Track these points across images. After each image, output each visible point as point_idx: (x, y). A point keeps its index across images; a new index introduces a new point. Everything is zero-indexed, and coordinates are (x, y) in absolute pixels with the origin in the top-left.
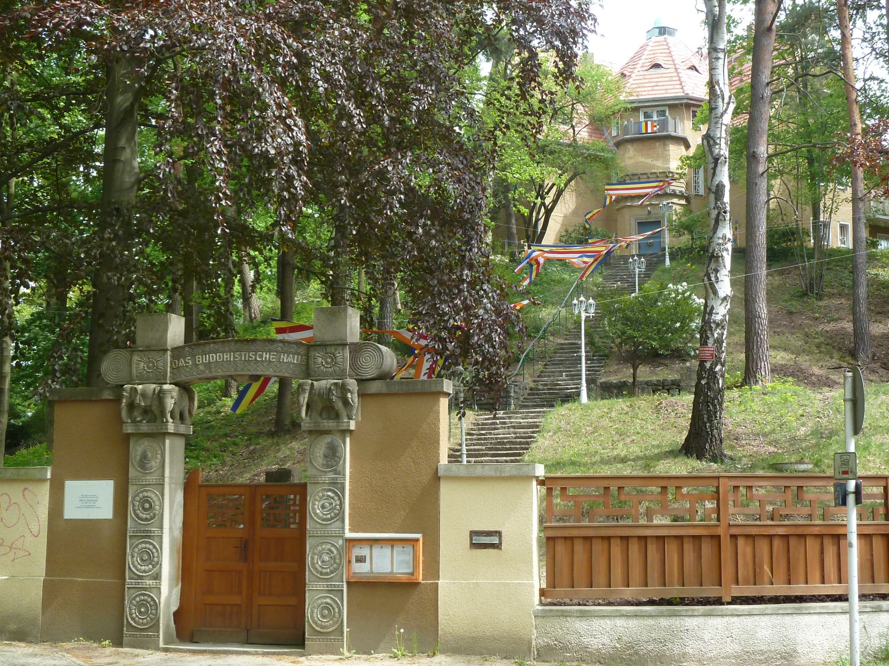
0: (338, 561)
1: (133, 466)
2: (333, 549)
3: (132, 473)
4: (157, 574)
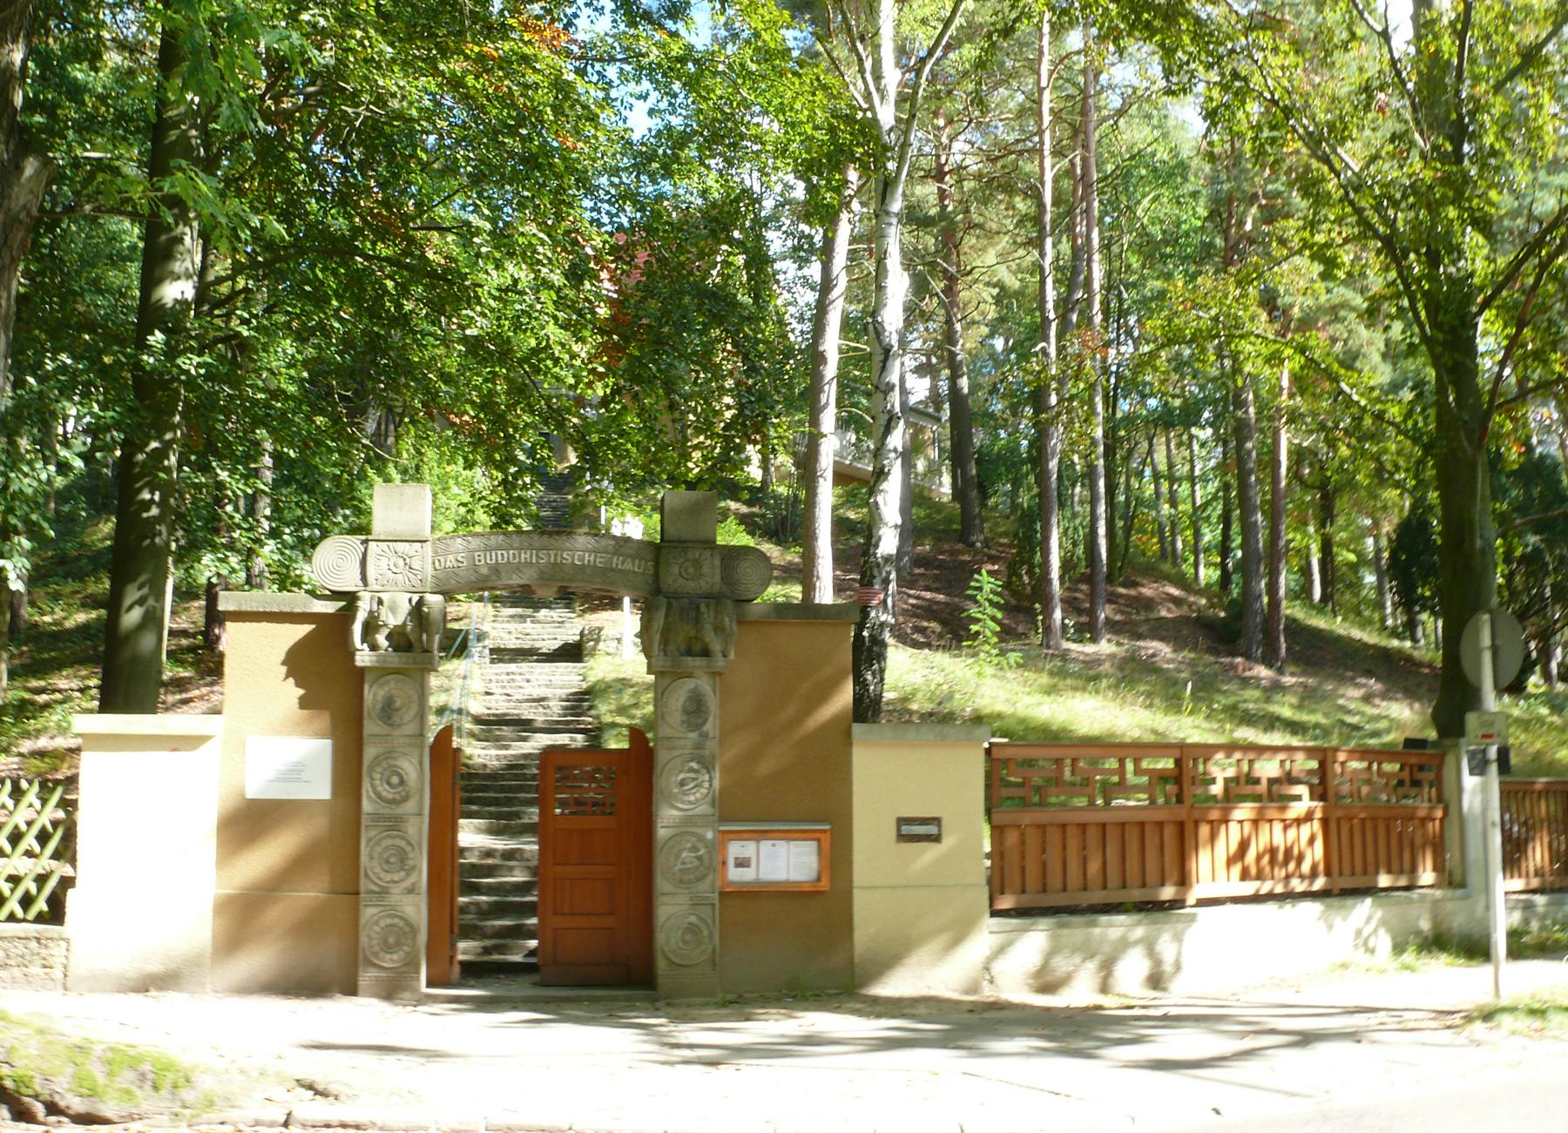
0: (706, 862)
2: (700, 845)
3: (371, 727)
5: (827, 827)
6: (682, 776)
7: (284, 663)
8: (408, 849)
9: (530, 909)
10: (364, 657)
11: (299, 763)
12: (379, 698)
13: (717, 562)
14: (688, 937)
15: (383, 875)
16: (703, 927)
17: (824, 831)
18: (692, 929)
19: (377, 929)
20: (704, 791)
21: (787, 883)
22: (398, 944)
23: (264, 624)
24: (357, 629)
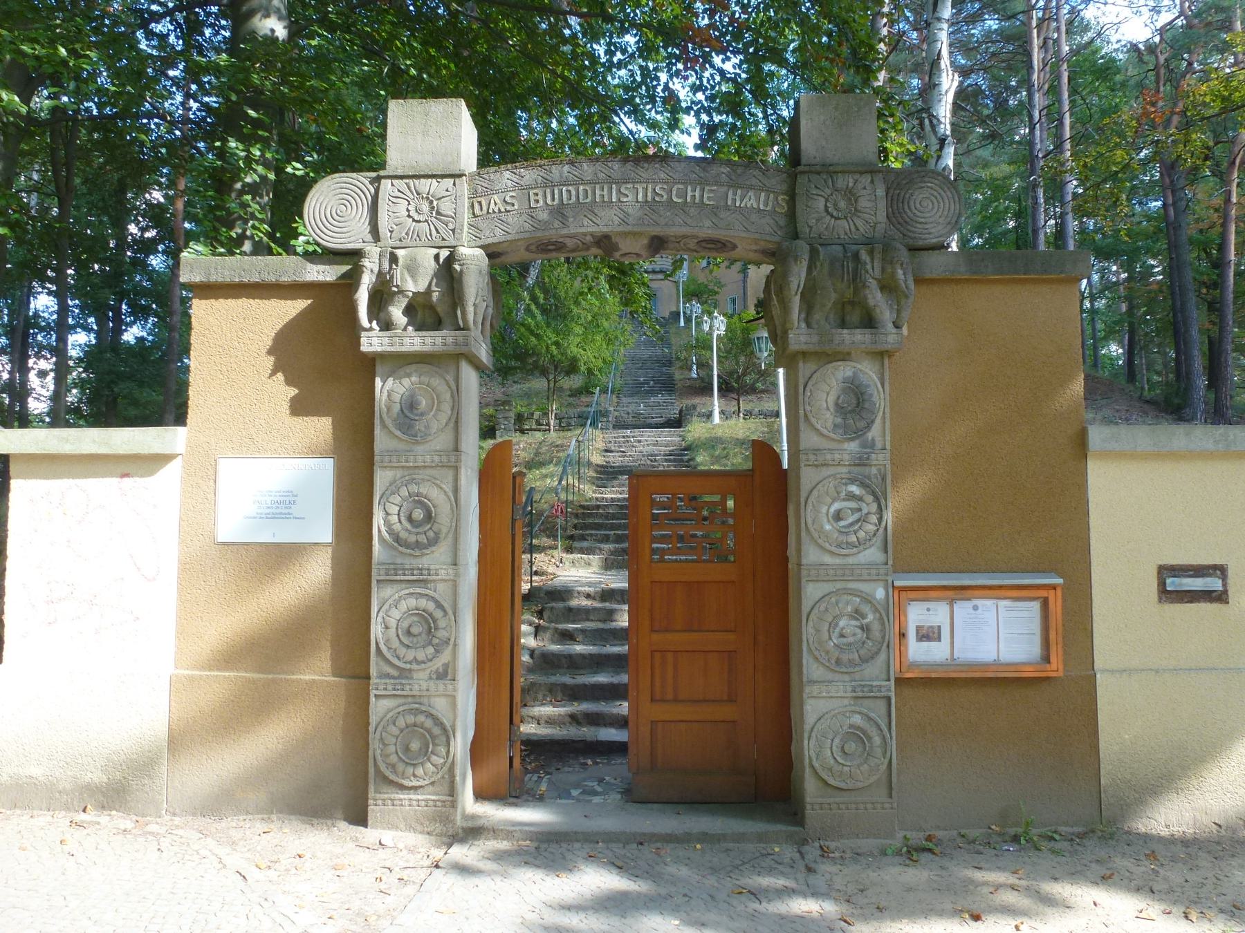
0: (876, 634)
1: (384, 426)
2: (866, 609)
3: (382, 441)
4: (446, 666)
5: (1061, 581)
6: (836, 506)
7: (270, 353)
8: (438, 614)
9: (615, 692)
10: (373, 341)
11: (290, 492)
12: (397, 397)
13: (881, 192)
14: (851, 747)
15: (402, 651)
16: (873, 732)
17: (1054, 587)
18: (858, 735)
19: (395, 731)
20: (871, 528)
21: (997, 664)
22: (425, 752)
23: (243, 302)
24: (362, 298)
